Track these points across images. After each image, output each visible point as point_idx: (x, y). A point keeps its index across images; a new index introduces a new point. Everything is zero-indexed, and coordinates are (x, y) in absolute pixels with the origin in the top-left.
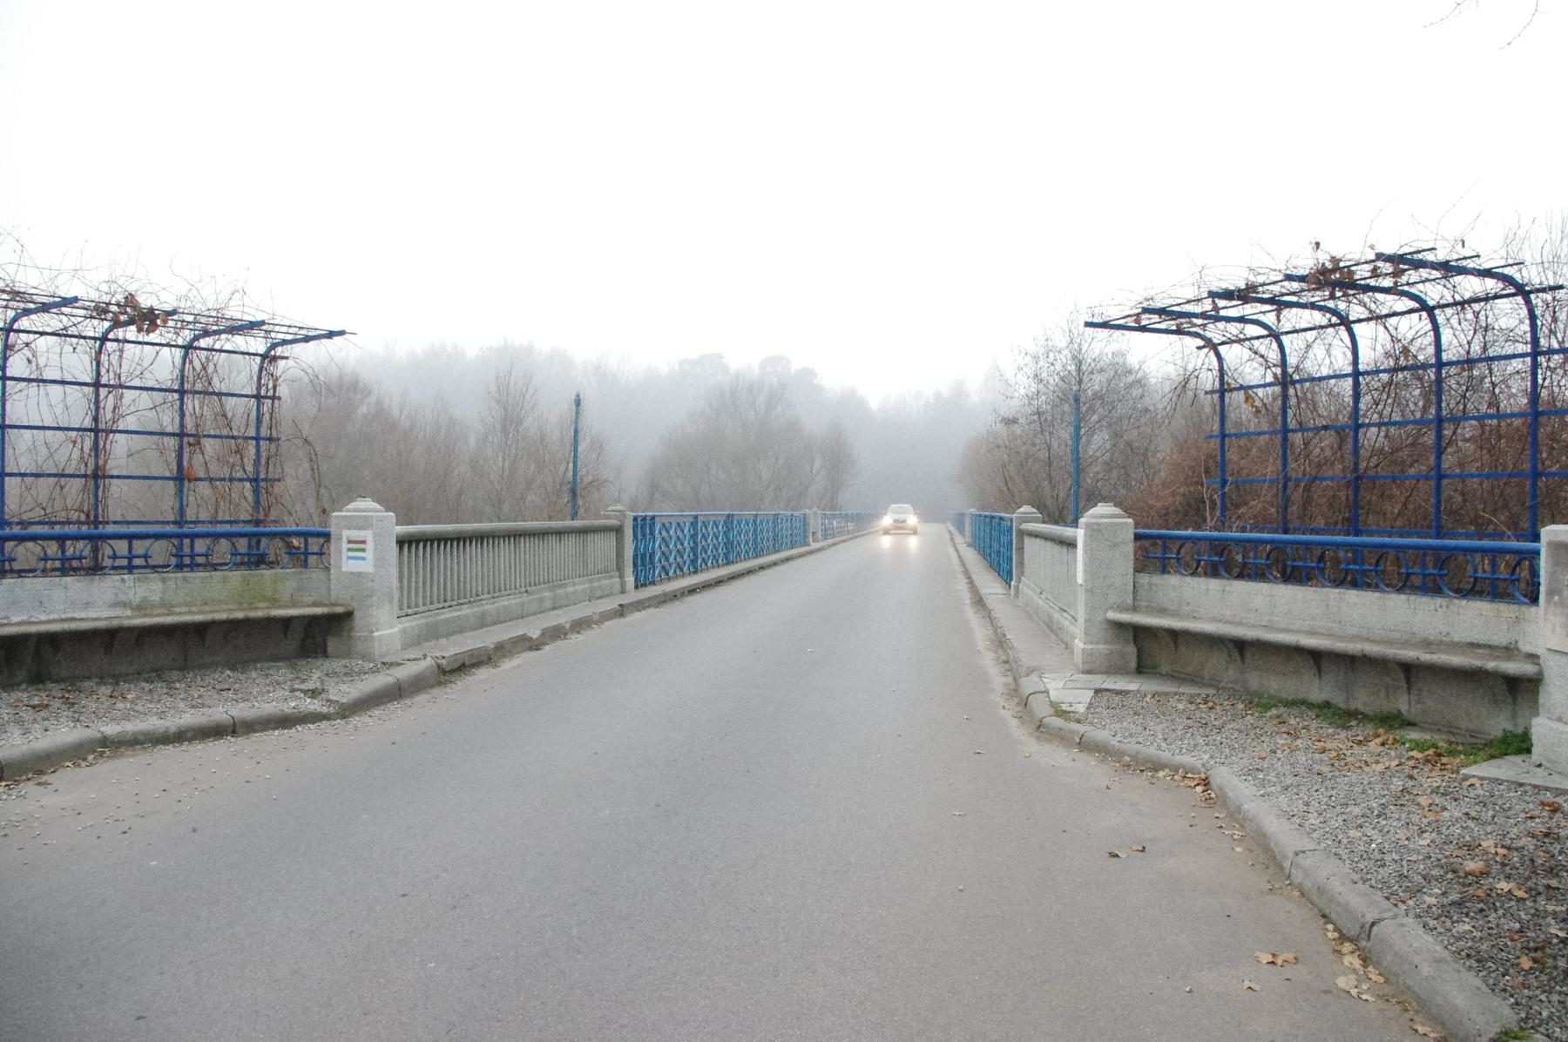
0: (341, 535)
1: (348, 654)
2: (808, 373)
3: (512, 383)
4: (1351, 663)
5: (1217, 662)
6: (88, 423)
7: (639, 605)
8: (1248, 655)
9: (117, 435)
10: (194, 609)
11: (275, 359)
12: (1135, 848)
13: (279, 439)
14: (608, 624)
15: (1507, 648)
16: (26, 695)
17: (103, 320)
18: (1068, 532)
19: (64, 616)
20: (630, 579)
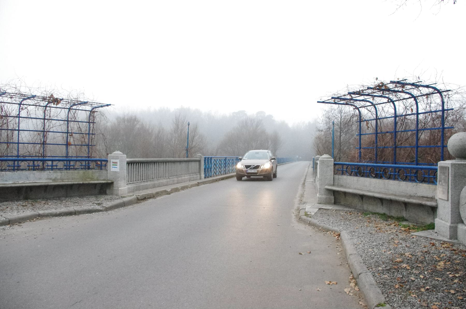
0: (111, 161)
1: (112, 194)
2: (270, 116)
3: (180, 118)
4: (391, 202)
5: (356, 201)
6: (42, 129)
7: (204, 183)
8: (364, 199)
9: (50, 133)
10: (70, 181)
11: (94, 112)
12: (308, 252)
13: (95, 134)
14: (193, 188)
15: (432, 198)
16: (22, 203)
17: (45, 101)
19: (33, 182)
20: (203, 176)
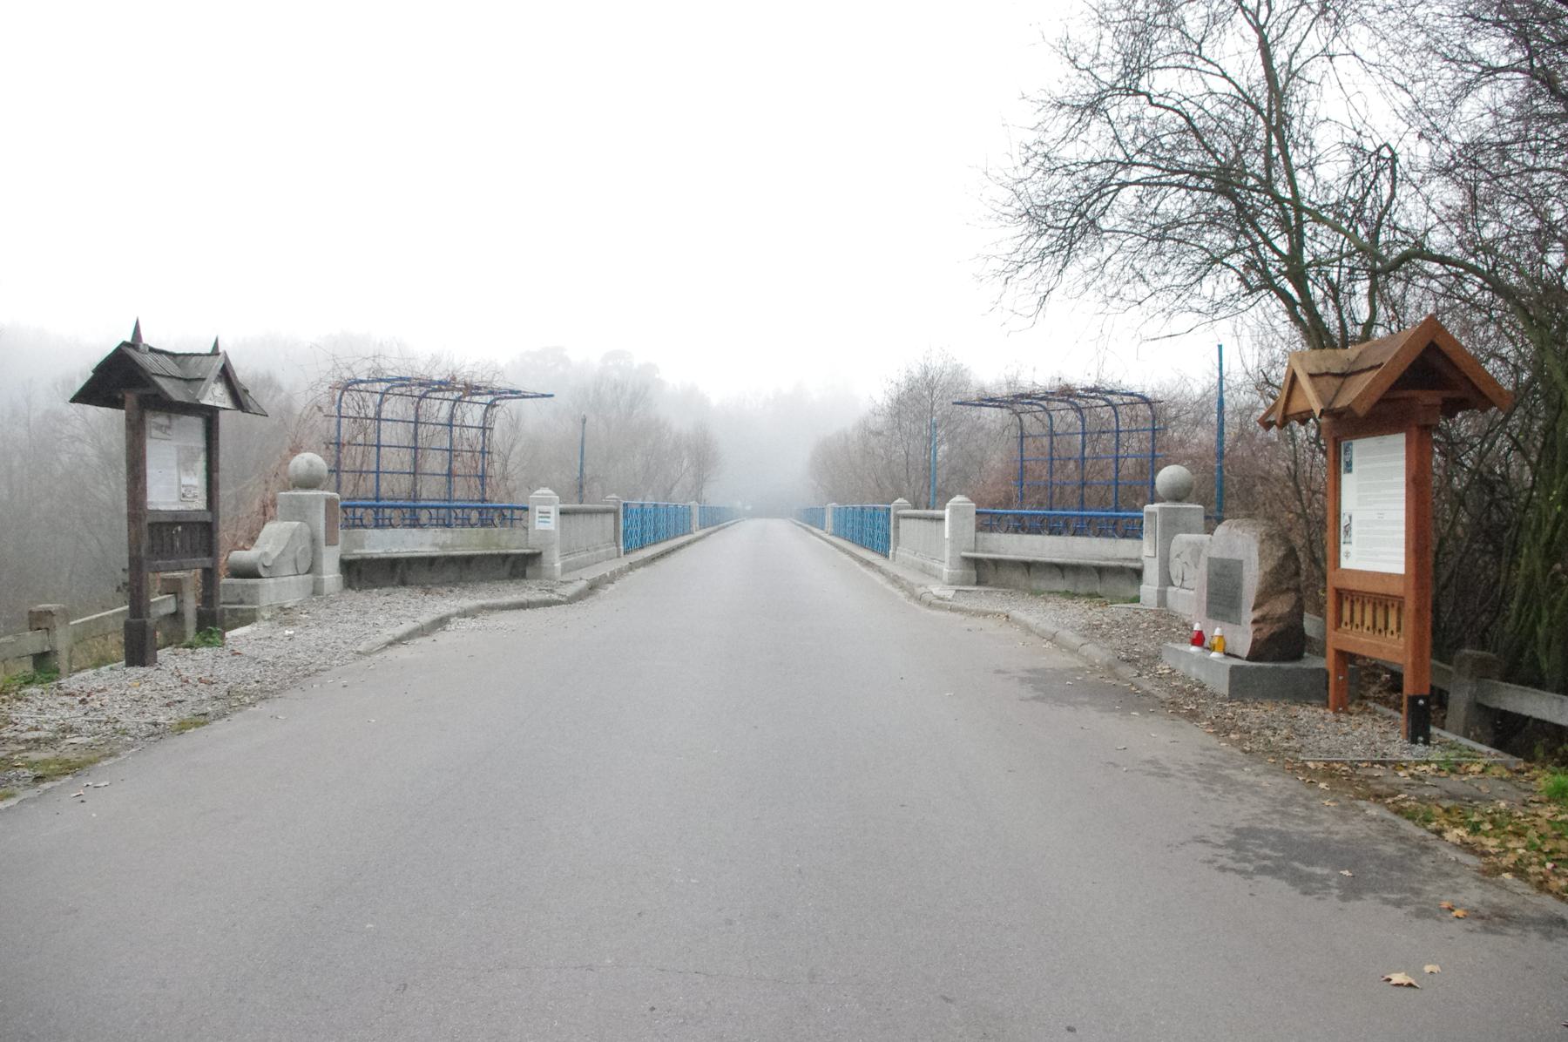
5: (1017, 576)
8: (1032, 570)
11: (495, 406)
18: (938, 512)
